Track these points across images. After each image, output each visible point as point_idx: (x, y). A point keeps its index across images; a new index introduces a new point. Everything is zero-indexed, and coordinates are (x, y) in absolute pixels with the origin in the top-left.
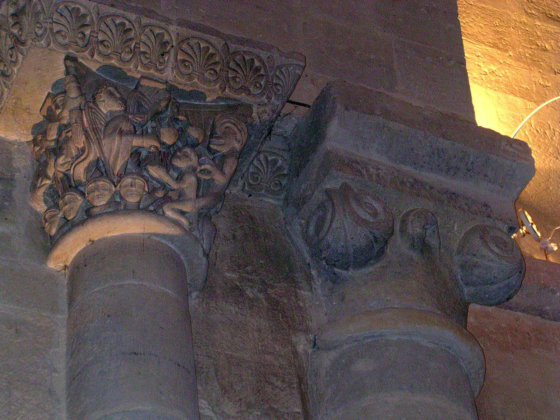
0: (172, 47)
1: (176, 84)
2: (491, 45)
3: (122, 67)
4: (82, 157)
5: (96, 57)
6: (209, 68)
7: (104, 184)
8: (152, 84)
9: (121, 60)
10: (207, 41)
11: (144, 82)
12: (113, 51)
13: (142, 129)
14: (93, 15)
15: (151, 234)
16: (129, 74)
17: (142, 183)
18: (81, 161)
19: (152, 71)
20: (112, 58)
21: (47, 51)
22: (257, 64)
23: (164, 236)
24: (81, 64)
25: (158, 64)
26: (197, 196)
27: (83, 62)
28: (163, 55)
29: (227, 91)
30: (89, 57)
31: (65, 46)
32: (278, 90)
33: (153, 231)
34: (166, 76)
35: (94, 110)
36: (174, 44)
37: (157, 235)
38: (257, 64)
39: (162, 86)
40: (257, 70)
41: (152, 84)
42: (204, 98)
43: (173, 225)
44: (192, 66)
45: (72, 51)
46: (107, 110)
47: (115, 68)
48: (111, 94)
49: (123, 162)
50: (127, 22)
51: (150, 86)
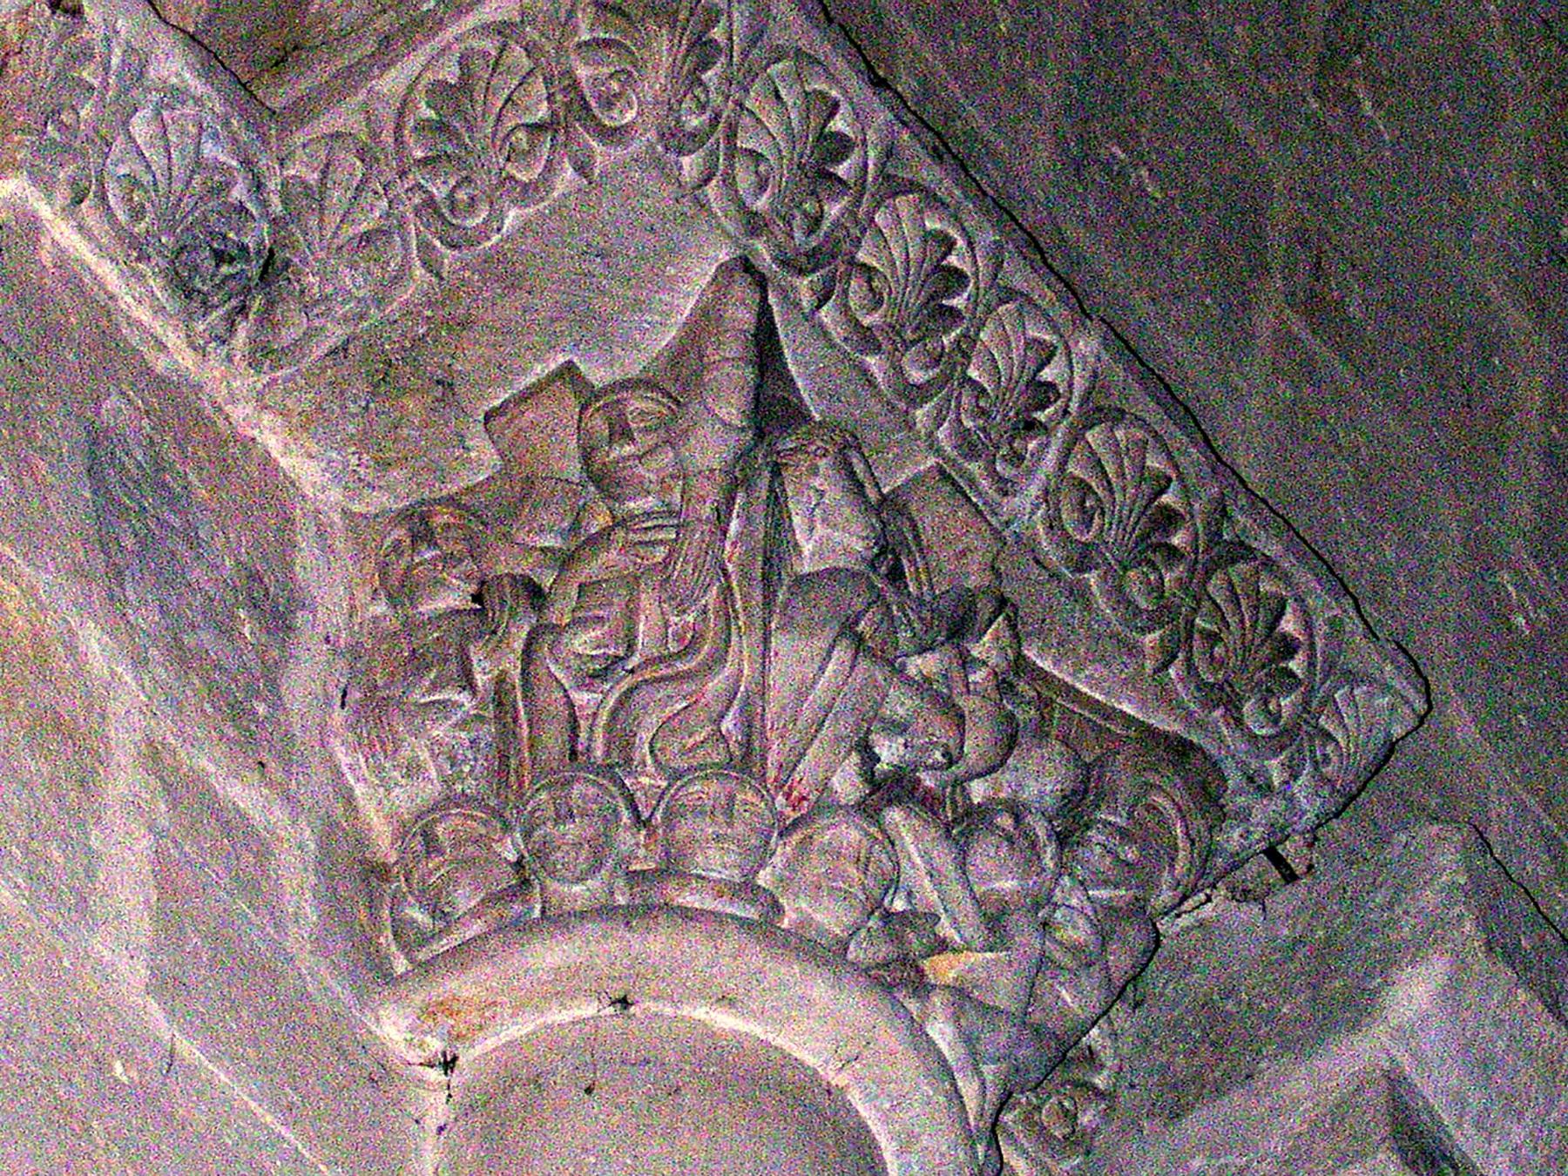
2: (382, 23)
4: (681, 666)
5: (827, 314)
9: (528, 192)
12: (889, 320)
13: (1206, 604)
14: (872, 154)
18: (671, 678)
21: (687, 206)
22: (1289, 625)
29: (1172, 671)
31: (754, 224)
32: (1326, 760)
38: (1289, 625)
40: (1288, 648)
44: (1103, 513)
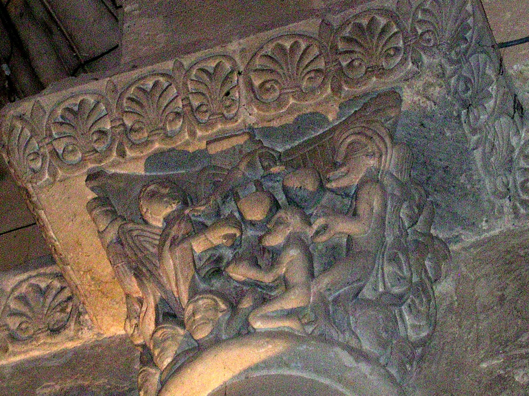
0: (239, 73)
1: (266, 124)
3: (174, 146)
5: (130, 154)
6: (305, 72)
7: (163, 333)
8: (226, 145)
10: (293, 35)
11: (215, 149)
15: (246, 371)
16: (191, 149)
17: (210, 301)
19: (219, 126)
20: (152, 142)
23: (266, 364)
24: (114, 175)
25: (225, 112)
26: (312, 275)
27: (118, 171)
28: (227, 94)
30: (122, 160)
33: (246, 365)
34: (244, 121)
35: (135, 233)
36: (242, 69)
37: (256, 367)
39: (241, 140)
41: (226, 145)
42: (325, 119)
43: (267, 339)
45: (93, 165)
46: (159, 221)
47: (162, 153)
48: (153, 195)
49: (187, 284)
50: (161, 79)
51: (224, 149)
